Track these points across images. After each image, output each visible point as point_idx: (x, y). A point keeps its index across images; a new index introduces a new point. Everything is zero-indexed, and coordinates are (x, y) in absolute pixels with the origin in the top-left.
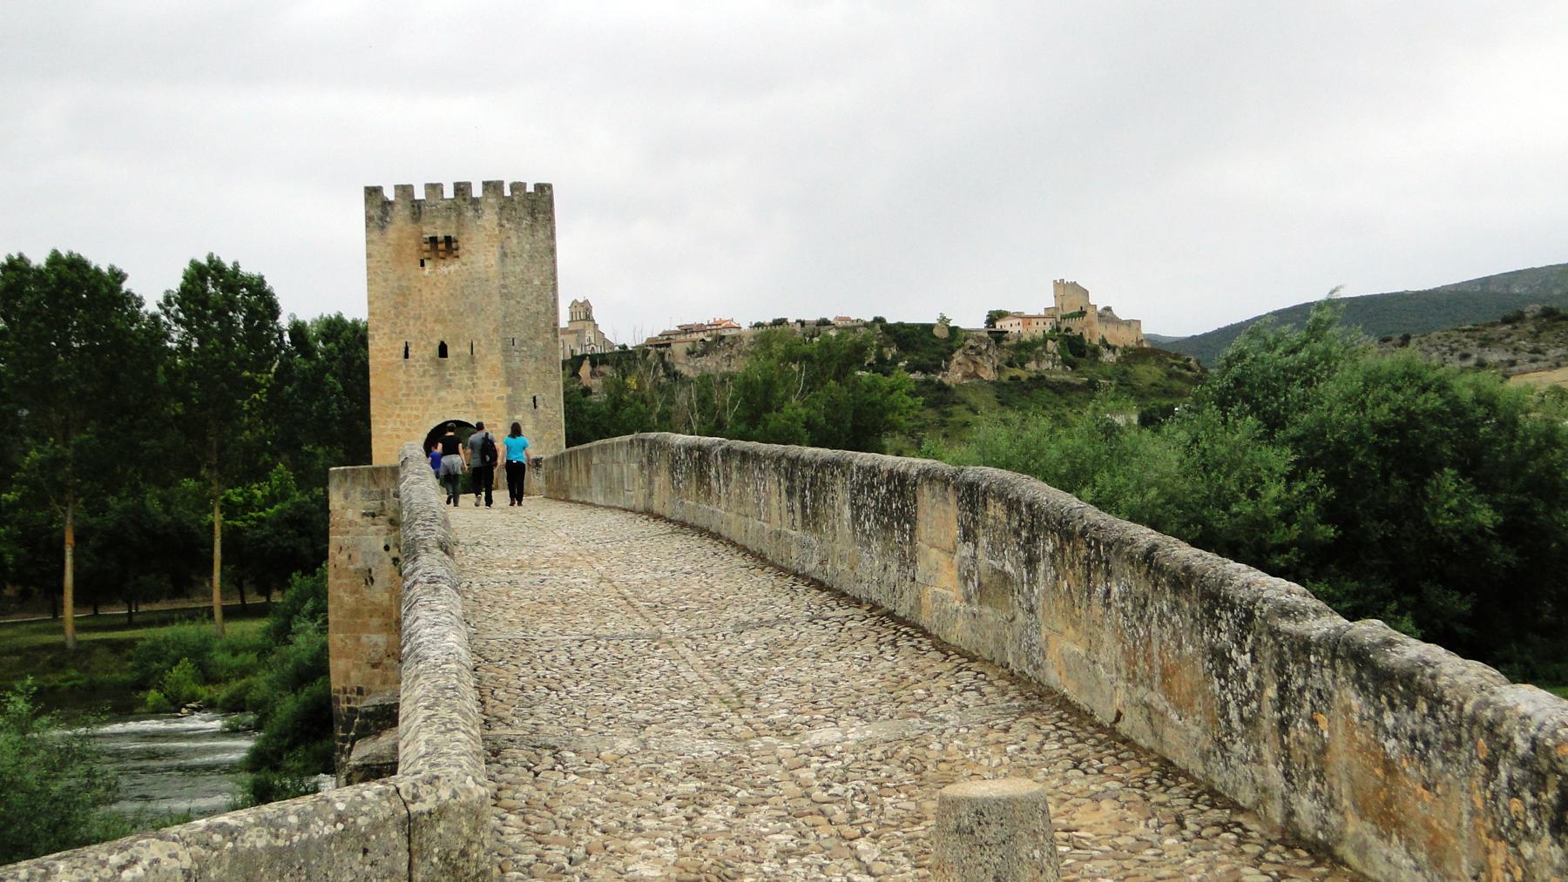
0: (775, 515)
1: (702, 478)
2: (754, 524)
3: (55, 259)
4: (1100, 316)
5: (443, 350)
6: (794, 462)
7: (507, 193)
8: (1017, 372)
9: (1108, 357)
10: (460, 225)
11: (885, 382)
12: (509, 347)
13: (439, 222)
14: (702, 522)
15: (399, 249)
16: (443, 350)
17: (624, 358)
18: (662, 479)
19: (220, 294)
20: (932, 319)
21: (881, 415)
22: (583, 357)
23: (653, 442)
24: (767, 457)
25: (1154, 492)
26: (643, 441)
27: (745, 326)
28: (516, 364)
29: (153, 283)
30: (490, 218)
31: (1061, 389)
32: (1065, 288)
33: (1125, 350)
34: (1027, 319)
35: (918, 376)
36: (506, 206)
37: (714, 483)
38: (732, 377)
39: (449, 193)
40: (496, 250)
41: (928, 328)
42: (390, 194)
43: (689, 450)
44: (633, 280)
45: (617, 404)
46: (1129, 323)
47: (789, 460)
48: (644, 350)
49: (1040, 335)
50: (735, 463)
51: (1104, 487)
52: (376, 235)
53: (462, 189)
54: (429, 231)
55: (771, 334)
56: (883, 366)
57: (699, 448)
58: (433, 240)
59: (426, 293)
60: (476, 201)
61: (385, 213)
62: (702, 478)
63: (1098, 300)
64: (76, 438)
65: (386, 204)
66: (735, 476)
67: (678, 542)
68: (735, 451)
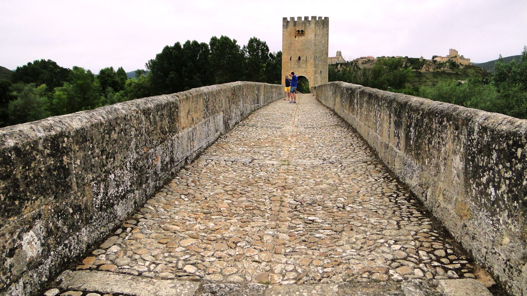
0: (386, 134)
1: (351, 103)
2: (372, 132)
3: (222, 37)
4: (460, 57)
5: (299, 58)
6: (403, 106)
7: (317, 19)
8: (438, 70)
9: (461, 67)
10: (305, 27)
11: (406, 71)
12: (315, 58)
13: (300, 26)
14: (349, 121)
15: (290, 33)
16: (299, 58)
17: (347, 64)
18: (338, 100)
19: (256, 45)
20: (419, 57)
21: (405, 78)
22: (339, 63)
23: (337, 85)
24: (385, 99)
25: (489, 103)
26: (334, 84)
27: (375, 58)
28: (317, 62)
29: (242, 42)
30: (313, 25)
31: (449, 74)
32: (452, 51)
33: (466, 66)
34: (442, 58)
35: (415, 70)
36: (317, 23)
37: (356, 106)
38: (371, 69)
39: (303, 19)
40: (314, 34)
41: (418, 59)
42: (289, 19)
43: (348, 89)
44: (348, 44)
45: (344, 74)
46: (467, 59)
47: (398, 103)
48: (352, 63)
49: (445, 61)
50: (366, 99)
51: (474, 101)
52: (285, 30)
53: (306, 18)
54: (297, 29)
55: (381, 60)
56: (406, 67)
57: (351, 89)
58: (299, 31)
59: (296, 45)
60: (309, 21)
61: (288, 24)
62: (351, 103)
63: (460, 54)
64: (225, 77)
65: (288, 22)
66: (365, 105)
67: (339, 133)
68: (366, 93)
